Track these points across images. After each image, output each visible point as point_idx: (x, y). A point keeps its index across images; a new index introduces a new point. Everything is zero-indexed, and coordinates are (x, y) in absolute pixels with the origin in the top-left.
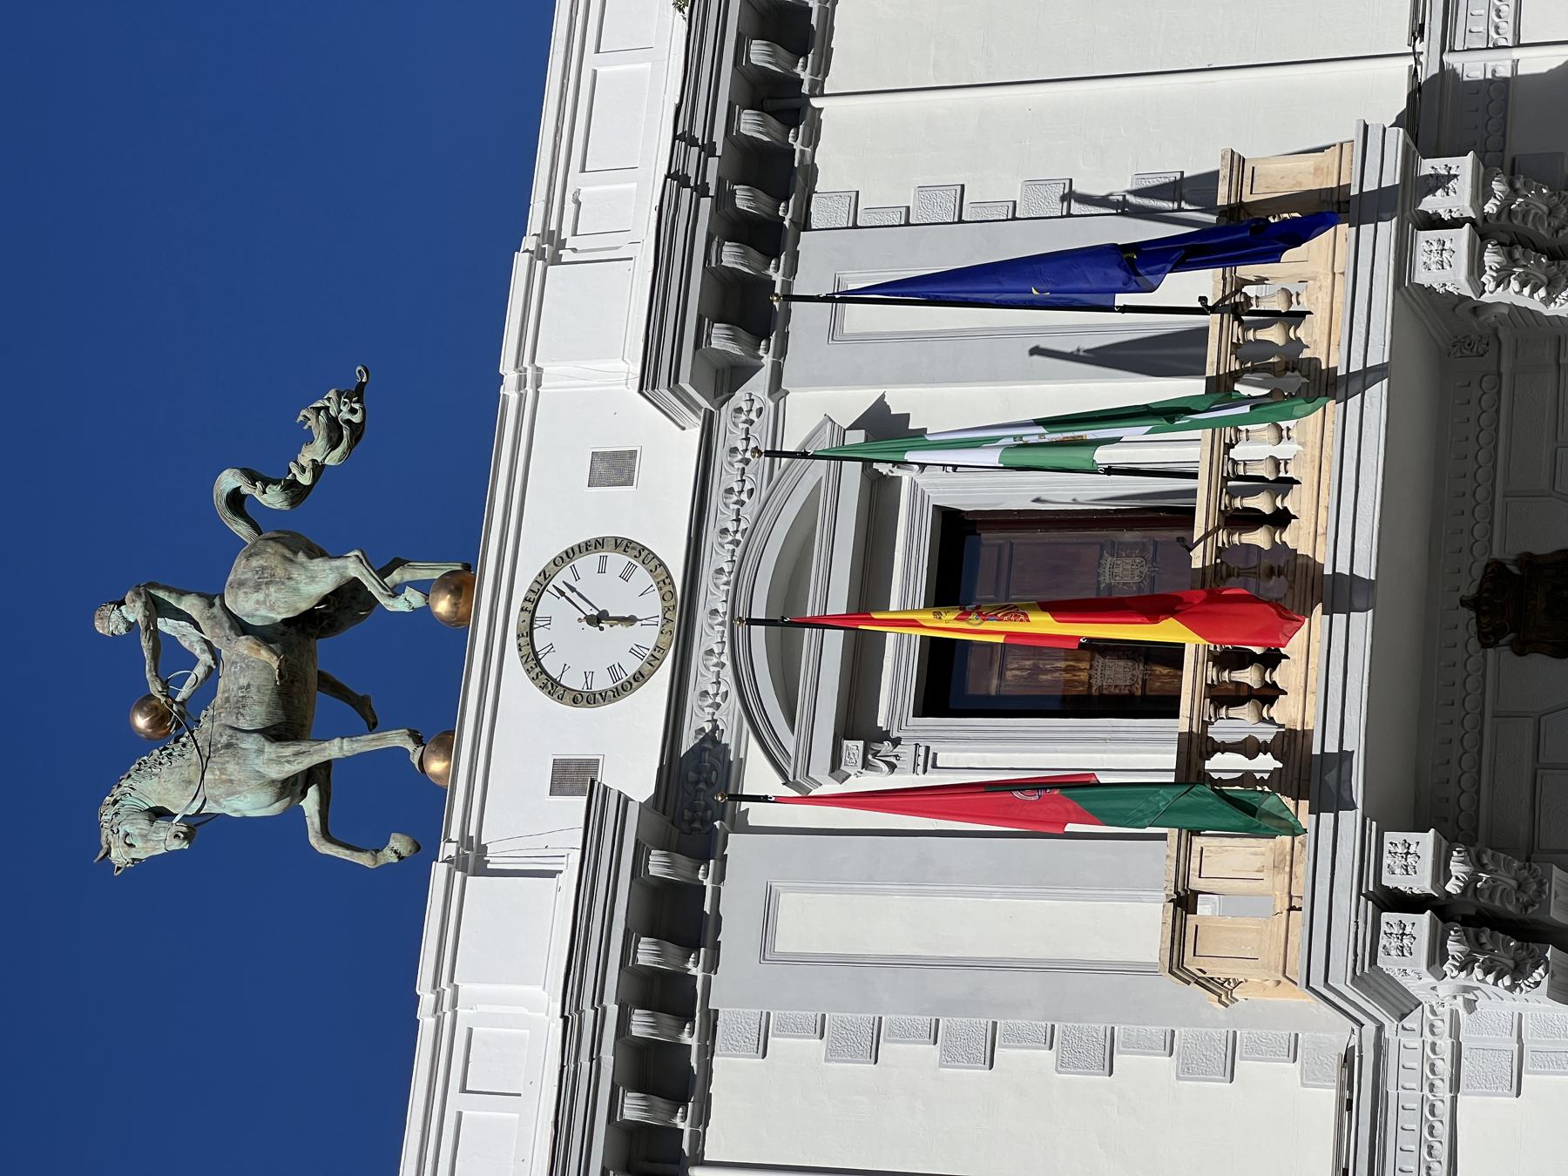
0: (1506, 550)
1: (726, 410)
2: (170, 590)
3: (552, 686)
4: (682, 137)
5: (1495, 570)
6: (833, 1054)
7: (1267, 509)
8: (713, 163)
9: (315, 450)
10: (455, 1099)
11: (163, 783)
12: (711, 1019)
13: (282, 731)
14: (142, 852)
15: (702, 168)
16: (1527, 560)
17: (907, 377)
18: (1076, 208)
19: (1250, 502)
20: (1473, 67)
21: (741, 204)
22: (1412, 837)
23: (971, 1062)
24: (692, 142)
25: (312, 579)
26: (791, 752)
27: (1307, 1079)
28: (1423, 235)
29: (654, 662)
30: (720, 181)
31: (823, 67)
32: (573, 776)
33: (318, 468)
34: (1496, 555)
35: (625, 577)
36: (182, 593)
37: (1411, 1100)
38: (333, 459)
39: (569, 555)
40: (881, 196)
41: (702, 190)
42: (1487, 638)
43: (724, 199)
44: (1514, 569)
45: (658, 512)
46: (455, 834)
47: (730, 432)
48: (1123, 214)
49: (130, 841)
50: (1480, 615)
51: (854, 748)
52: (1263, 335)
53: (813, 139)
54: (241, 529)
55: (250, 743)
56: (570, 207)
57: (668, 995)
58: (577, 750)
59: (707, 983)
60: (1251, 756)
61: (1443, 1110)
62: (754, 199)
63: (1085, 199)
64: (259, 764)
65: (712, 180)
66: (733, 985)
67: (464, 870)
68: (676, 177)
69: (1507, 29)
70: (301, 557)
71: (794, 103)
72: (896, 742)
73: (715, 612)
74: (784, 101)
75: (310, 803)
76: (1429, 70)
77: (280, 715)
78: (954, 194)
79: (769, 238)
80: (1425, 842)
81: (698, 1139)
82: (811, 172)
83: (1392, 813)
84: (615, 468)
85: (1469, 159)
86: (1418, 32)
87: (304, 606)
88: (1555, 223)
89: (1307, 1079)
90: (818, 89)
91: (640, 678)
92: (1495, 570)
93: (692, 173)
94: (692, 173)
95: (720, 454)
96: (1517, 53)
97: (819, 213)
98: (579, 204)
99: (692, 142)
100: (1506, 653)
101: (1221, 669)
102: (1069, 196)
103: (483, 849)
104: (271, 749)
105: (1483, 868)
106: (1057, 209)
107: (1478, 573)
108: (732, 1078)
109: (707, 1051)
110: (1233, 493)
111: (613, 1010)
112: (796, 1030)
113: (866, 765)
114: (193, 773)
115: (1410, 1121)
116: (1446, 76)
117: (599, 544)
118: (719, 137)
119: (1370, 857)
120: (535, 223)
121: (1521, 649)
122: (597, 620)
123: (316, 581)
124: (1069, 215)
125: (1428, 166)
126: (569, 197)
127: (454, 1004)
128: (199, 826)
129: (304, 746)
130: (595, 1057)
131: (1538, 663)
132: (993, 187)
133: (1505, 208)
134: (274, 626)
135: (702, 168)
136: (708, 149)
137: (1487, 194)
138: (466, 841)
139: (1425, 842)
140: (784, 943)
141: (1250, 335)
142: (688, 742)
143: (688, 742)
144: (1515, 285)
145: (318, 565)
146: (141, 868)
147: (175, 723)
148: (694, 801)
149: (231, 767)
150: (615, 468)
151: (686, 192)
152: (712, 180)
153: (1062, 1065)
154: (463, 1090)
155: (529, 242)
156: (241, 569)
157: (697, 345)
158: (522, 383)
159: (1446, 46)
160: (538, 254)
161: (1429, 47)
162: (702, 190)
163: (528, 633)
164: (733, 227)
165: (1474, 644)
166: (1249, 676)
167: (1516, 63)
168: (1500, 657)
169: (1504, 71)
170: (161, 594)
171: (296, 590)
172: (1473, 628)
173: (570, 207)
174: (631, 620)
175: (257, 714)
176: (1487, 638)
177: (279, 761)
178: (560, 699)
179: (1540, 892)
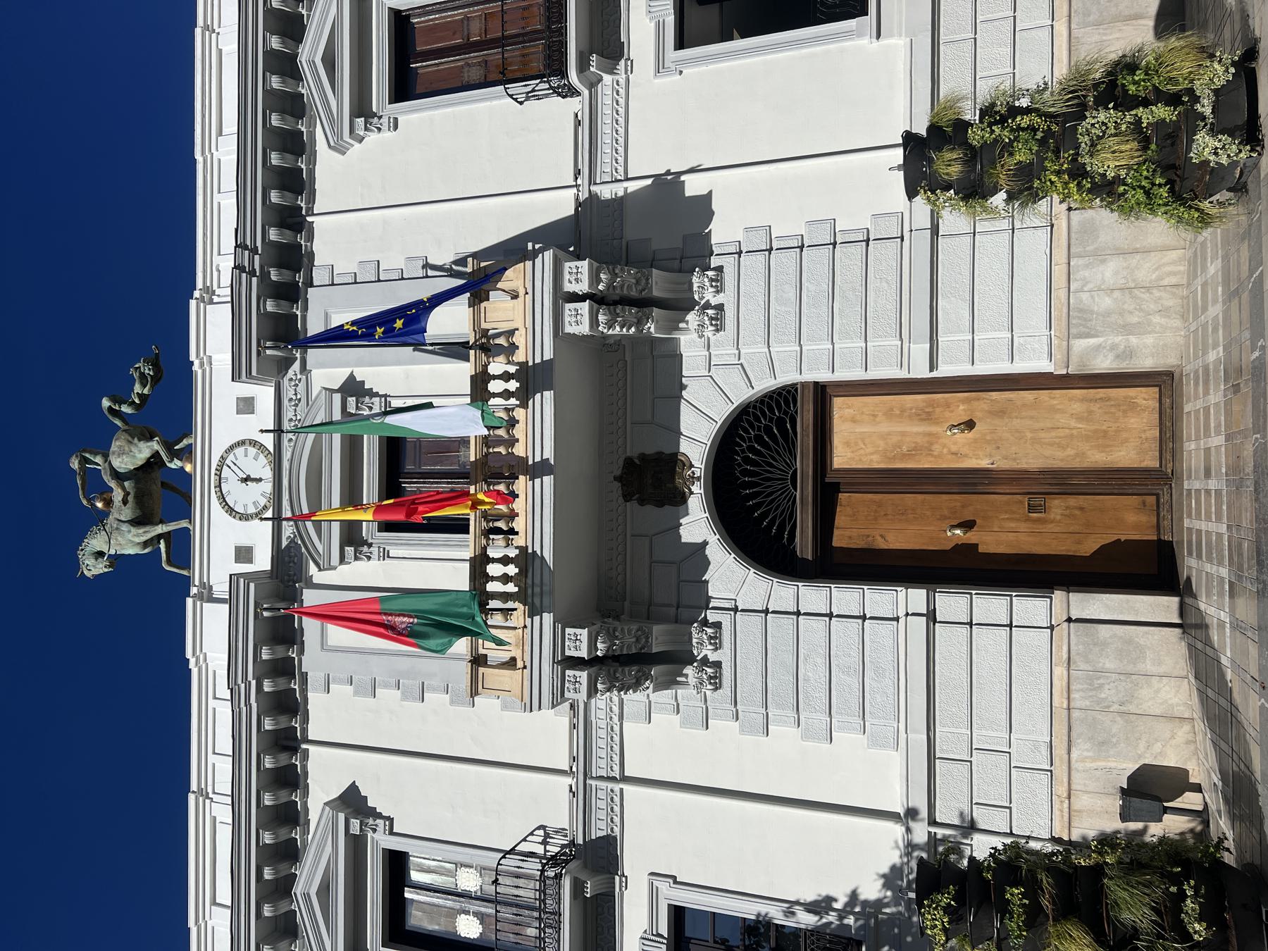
0: (633, 451)
1: (286, 379)
2: (91, 453)
3: (231, 511)
4: (240, 246)
5: (629, 462)
6: (356, 693)
9: (137, 388)
10: (212, 703)
11: (96, 542)
12: (304, 677)
13: (137, 522)
14: (96, 572)
15: (252, 261)
16: (643, 457)
17: (360, 364)
18: (430, 273)
20: (606, 192)
21: (274, 278)
22: (578, 631)
23: (414, 700)
24: (246, 247)
25: (140, 451)
28: (568, 306)
30: (262, 267)
31: (312, 199)
33: (140, 396)
34: (629, 454)
36: (96, 454)
37: (602, 724)
38: (146, 391)
39: (232, 448)
40: (345, 267)
41: (252, 273)
42: (627, 497)
43: (265, 276)
44: (637, 461)
46: (197, 583)
47: (289, 392)
48: (451, 276)
49: (94, 568)
50: (623, 485)
51: (350, 550)
53: (310, 238)
54: (118, 422)
55: (125, 527)
56: (215, 274)
57: (284, 669)
58: (245, 542)
59: (300, 661)
60: (505, 584)
61: (617, 728)
62: (280, 275)
63: (434, 267)
64: (130, 536)
65: (257, 267)
66: (312, 661)
67: (202, 599)
68: (238, 267)
69: (621, 170)
70: (136, 440)
71: (299, 219)
72: (370, 545)
74: (293, 220)
75: (162, 546)
76: (584, 195)
77: (138, 513)
78: (374, 265)
79: (291, 293)
80: (584, 633)
81: (305, 731)
82: (311, 255)
83: (566, 620)
85: (586, 262)
86: (577, 173)
87: (140, 463)
88: (640, 288)
90: (310, 212)
92: (629, 462)
93: (246, 264)
94: (246, 264)
95: (285, 402)
96: (626, 184)
97: (319, 276)
98: (219, 271)
99: (246, 247)
100: (635, 504)
102: (426, 266)
103: (211, 588)
104: (134, 530)
105: (617, 638)
106: (421, 273)
107: (621, 463)
108: (316, 702)
109: (304, 691)
111: (254, 683)
112: (340, 682)
113: (356, 558)
115: (602, 733)
116: (593, 197)
117: (242, 443)
118: (259, 244)
119: (559, 641)
120: (199, 284)
121: (642, 502)
122: (246, 480)
123: (143, 451)
124: (427, 277)
127: (205, 660)
128: (116, 560)
129: (147, 528)
130: (248, 703)
131: (650, 509)
132: (393, 261)
133: (609, 286)
134: (131, 471)
135: (252, 261)
136: (254, 251)
137: (599, 281)
138: (202, 585)
139: (584, 633)
142: (284, 543)
143: (284, 543)
144: (618, 328)
145: (142, 445)
146: (96, 577)
147: (99, 519)
148: (288, 572)
150: (246, 405)
151: (244, 275)
152: (257, 267)
153: (452, 702)
154: (215, 698)
155: (197, 294)
156: (115, 446)
157: (259, 353)
158: (202, 365)
159: (592, 182)
160: (202, 299)
161: (583, 180)
162: (252, 273)
165: (621, 500)
167: (626, 189)
168: (632, 506)
169: (621, 193)
170: (87, 455)
171: (134, 457)
172: (620, 492)
173: (215, 274)
174: (260, 480)
175: (127, 513)
176: (627, 497)
177: (138, 535)
179: (647, 641)
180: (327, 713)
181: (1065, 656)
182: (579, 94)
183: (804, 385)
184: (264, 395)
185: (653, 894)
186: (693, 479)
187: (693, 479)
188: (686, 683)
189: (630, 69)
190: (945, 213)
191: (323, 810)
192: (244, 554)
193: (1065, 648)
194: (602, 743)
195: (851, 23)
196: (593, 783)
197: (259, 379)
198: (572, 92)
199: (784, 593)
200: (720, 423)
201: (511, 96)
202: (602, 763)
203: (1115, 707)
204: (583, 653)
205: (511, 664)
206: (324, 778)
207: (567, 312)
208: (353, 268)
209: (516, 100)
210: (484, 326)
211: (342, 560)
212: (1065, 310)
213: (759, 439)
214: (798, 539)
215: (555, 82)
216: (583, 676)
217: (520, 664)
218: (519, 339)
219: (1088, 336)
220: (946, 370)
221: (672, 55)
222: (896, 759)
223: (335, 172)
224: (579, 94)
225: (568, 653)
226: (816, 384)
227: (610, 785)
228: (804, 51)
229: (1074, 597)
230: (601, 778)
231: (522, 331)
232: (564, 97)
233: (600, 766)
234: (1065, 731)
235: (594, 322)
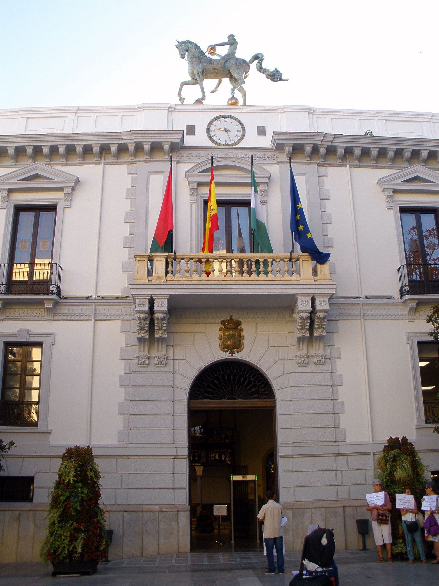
7: (244, 269)
8: (330, 144)
12: (135, 163)
19: (245, 266)
26: (194, 173)
27: (123, 289)
29: (217, 143)
32: (191, 130)
35: (237, 136)
44: (239, 327)
45: (252, 140)
52: (245, 266)
66: (143, 166)
73: (237, 154)
81: (109, 163)
84: (262, 131)
89: (123, 289)
91: (213, 141)
101: (263, 262)
110: (247, 262)
113: (191, 190)
114: (196, 56)
115: (115, 311)
125: (53, 288)
126: (325, 116)
140: (151, 176)
141: (245, 263)
149: (196, 63)
150: (262, 131)
153: (125, 237)
161: (359, 317)
163: (223, 116)
164: (315, 149)
166: (245, 268)
173: (323, 116)
178: (208, 125)
180: (118, 175)
181: (164, 510)
182: (401, 298)
183: (274, 402)
184: (266, 142)
185: (48, 335)
186: (232, 353)
187: (232, 353)
188: (140, 351)
189: (410, 320)
190: (398, 496)
191: (75, 176)
192: (191, 130)
193: (167, 510)
194: (111, 311)
195: (423, 417)
196: (93, 307)
197: (274, 140)
198: (402, 293)
199: (183, 395)
200: (257, 365)
201: (400, 267)
202: (102, 311)
203: (145, 528)
204: (156, 308)
205: (150, 273)
206: (88, 172)
207: (307, 299)
208: (326, 188)
209: (399, 269)
210: (301, 260)
211: (190, 183)
212: (304, 507)
213: (245, 379)
214: (205, 400)
215: (407, 289)
216: (146, 308)
217: (150, 278)
218: (295, 276)
219: (293, 516)
220: (346, 457)
221: (416, 340)
222: (114, 442)
223: (369, 179)
224: (401, 298)
225: (155, 300)
226: (275, 407)
227: (93, 315)
228: (413, 398)
229: (188, 514)
230: (95, 310)
231: (299, 278)
232: (400, 290)
233: (100, 310)
234: (133, 510)
235: (303, 311)
